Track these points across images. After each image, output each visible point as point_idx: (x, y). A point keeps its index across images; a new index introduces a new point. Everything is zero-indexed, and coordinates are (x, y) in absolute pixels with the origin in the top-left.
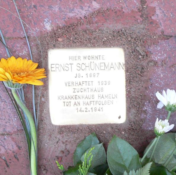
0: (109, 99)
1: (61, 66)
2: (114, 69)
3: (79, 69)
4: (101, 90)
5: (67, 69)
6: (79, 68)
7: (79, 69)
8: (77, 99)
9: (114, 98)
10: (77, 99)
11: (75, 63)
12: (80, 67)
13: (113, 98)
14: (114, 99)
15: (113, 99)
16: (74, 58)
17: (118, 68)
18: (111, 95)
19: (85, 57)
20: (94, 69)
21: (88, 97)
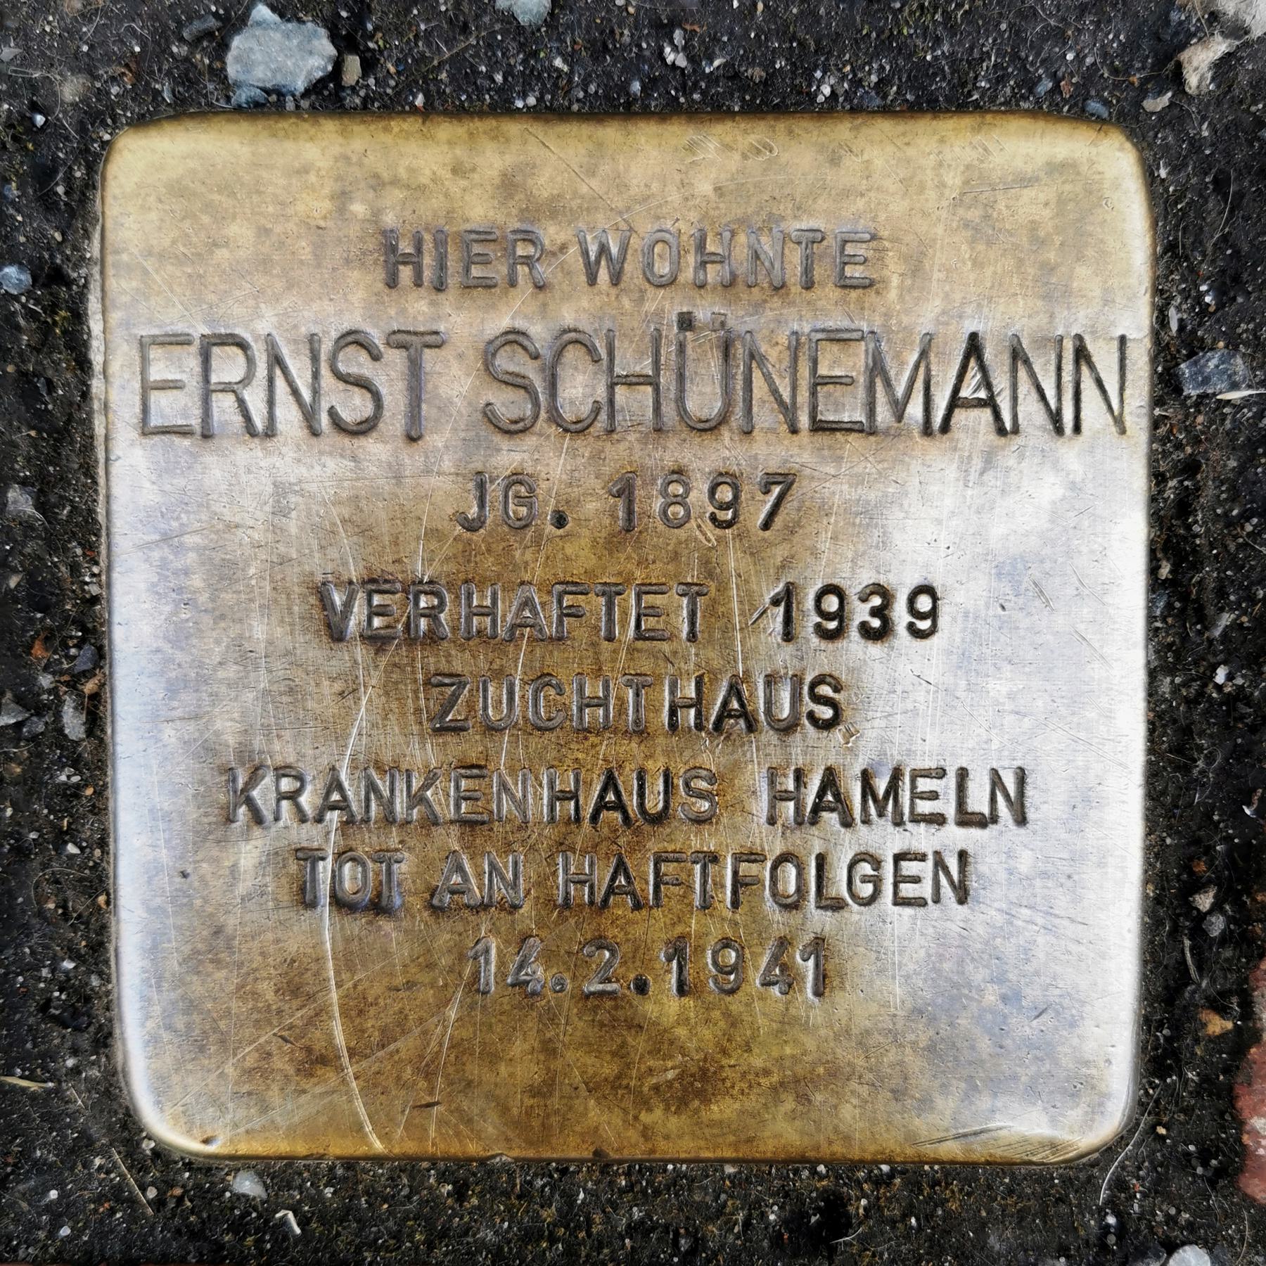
0: (922, 838)
1: (276, 360)
2: (1001, 431)
3: (509, 404)
4: (808, 705)
5: (355, 407)
6: (342, 368)
7: (509, 404)
8: (920, 902)
9: (982, 822)
10: (920, 902)
11: (466, 323)
12: (527, 388)
13: (966, 819)
14: (992, 830)
15: (975, 832)
16: (453, 264)
17: (1056, 418)
18: (947, 786)
19: (603, 250)
20: (723, 419)
21: (632, 803)
